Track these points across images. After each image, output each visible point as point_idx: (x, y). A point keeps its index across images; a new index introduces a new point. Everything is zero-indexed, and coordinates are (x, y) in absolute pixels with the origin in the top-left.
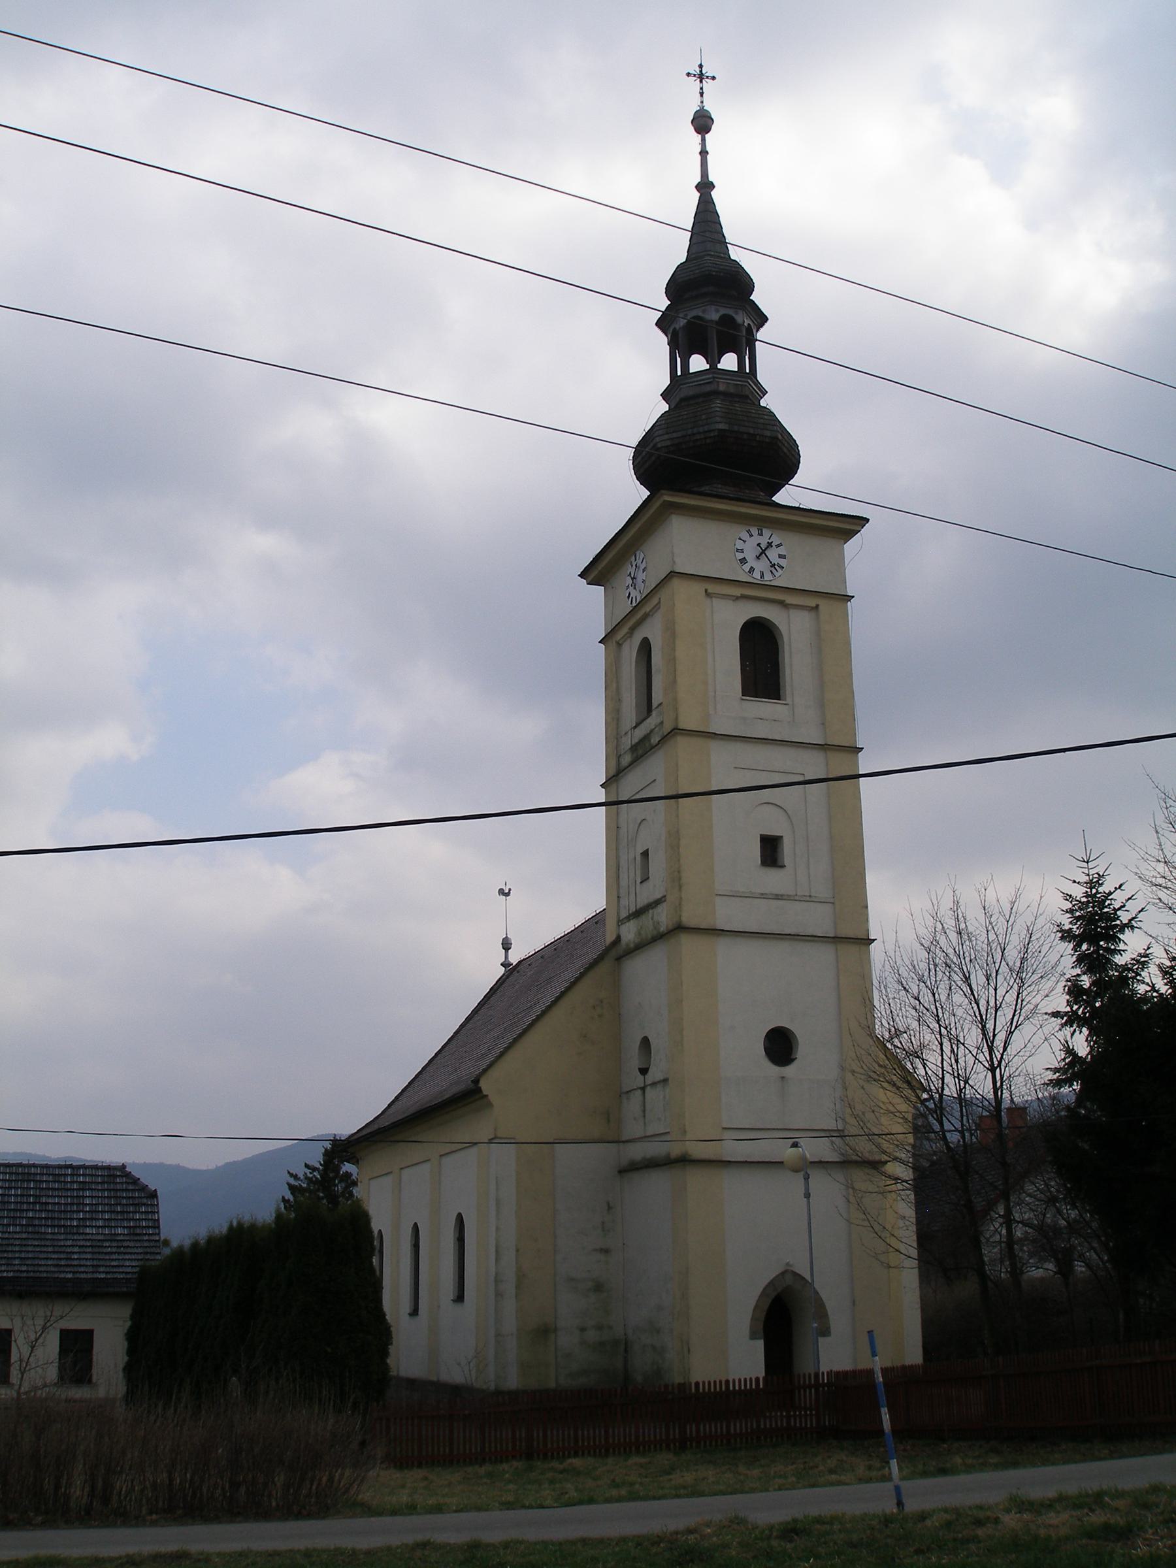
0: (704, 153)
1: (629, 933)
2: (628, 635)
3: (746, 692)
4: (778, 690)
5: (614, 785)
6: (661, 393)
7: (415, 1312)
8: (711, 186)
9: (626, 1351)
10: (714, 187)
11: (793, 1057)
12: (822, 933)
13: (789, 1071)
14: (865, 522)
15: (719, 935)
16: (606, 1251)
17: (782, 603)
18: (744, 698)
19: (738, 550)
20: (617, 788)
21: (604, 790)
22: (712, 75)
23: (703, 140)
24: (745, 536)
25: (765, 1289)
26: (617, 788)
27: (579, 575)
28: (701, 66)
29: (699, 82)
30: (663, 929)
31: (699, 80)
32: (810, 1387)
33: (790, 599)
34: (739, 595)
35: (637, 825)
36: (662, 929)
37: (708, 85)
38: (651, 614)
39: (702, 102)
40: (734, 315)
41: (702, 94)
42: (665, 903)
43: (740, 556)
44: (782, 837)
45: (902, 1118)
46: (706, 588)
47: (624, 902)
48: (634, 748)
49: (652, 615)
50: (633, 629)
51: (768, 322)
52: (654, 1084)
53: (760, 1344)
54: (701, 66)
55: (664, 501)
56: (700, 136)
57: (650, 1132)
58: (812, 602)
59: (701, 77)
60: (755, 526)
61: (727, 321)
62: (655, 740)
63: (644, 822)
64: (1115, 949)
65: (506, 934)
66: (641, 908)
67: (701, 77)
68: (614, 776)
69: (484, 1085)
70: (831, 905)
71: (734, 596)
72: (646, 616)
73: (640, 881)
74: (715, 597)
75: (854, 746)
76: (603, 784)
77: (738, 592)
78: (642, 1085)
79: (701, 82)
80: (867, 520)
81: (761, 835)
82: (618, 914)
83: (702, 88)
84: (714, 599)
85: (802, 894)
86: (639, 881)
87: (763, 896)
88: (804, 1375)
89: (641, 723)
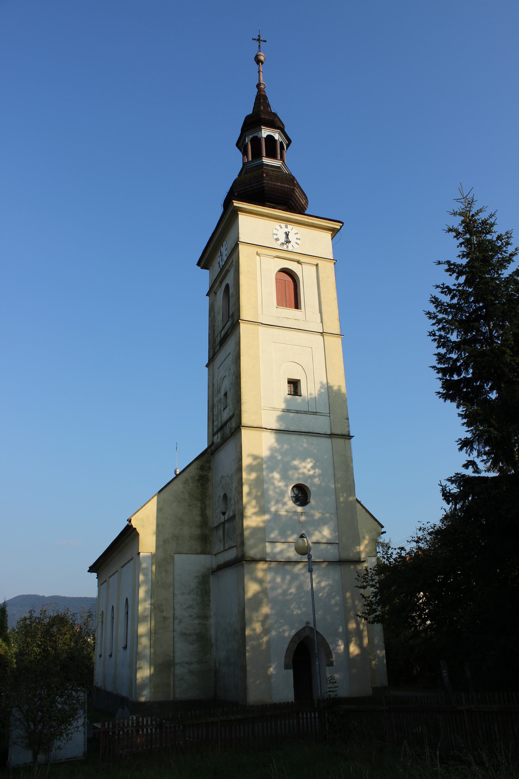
2: (219, 286)
4: (298, 307)
7: (125, 648)
11: (308, 501)
12: (324, 432)
18: (277, 307)
24: (278, 227)
28: (259, 36)
40: (273, 135)
43: (275, 237)
44: (300, 380)
45: (214, 352)
49: (230, 270)
50: (221, 282)
53: (291, 672)
54: (259, 36)
58: (315, 261)
63: (226, 377)
64: (367, 606)
69: (134, 524)
70: (329, 417)
73: (223, 409)
79: (259, 43)
83: (259, 46)
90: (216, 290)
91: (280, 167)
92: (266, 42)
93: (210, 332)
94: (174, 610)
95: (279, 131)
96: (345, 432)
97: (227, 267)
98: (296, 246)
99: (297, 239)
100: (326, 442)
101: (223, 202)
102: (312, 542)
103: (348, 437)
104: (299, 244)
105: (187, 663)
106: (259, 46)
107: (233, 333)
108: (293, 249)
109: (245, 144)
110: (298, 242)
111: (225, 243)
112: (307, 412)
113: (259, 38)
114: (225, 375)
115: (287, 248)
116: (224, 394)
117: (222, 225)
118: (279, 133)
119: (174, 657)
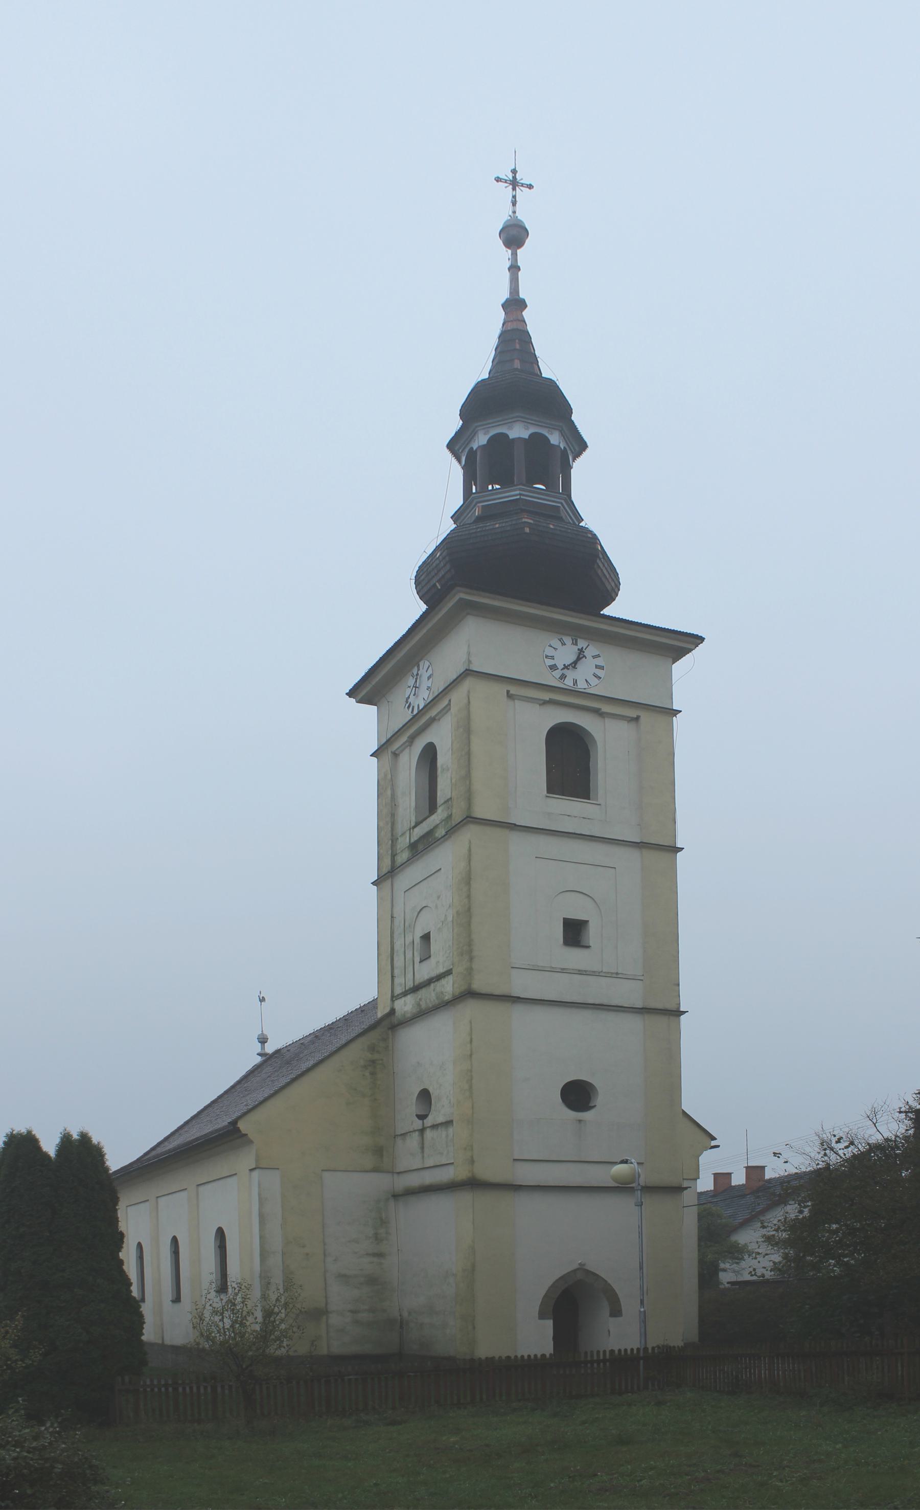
0: (514, 269)
1: (405, 1006)
3: (550, 790)
4: (589, 793)
5: (388, 882)
6: (451, 515)
7: (177, 1299)
8: (522, 305)
9: (401, 1327)
10: (526, 306)
11: (591, 1104)
13: (586, 1115)
14: (700, 641)
15: (514, 1002)
16: (380, 1255)
17: (597, 712)
18: (548, 795)
19: (547, 657)
20: (392, 885)
21: (376, 887)
22: (528, 183)
23: (514, 255)
25: (557, 1281)
26: (392, 885)
27: (347, 694)
28: (514, 172)
29: (511, 190)
30: (447, 997)
31: (511, 187)
32: (598, 1362)
33: (606, 708)
34: (548, 699)
35: (416, 914)
36: (446, 998)
37: (521, 193)
38: (437, 718)
39: (514, 212)
40: (547, 435)
41: (514, 203)
42: (451, 975)
43: (549, 662)
44: (588, 921)
46: (509, 689)
47: (399, 980)
48: (413, 846)
49: (439, 720)
50: (412, 739)
51: (588, 451)
52: (434, 1127)
53: (549, 1323)
54: (514, 172)
55: (461, 599)
56: (510, 251)
57: (430, 1162)
58: (632, 713)
59: (515, 183)
60: (569, 635)
61: (538, 441)
62: (440, 832)
65: (261, 1005)
66: (420, 984)
67: (515, 183)
68: (389, 872)
71: (542, 700)
72: (433, 720)
74: (519, 700)
75: (674, 846)
76: (374, 882)
77: (546, 696)
78: (420, 1127)
79: (514, 189)
80: (701, 639)
81: (564, 918)
82: (392, 991)
83: (514, 197)
84: (516, 701)
85: (606, 971)
86: (417, 959)
87: (563, 971)
88: (592, 1352)
89: (421, 822)
90: (398, 748)
91: (558, 507)
92: (532, 190)
93: (381, 824)
94: (325, 1244)
95: (561, 424)
96: (671, 1006)
97: (433, 713)
98: (593, 681)
99: (597, 667)
100: (634, 1023)
101: (415, 574)
102: (638, 1162)
103: (678, 1013)
104: (600, 678)
105: (351, 1311)
106: (514, 197)
107: (450, 837)
108: (587, 687)
109: (472, 448)
110: (600, 673)
111: (428, 663)
112: (599, 972)
113: (514, 178)
114: (424, 905)
115: (574, 685)
116: (421, 935)
117: (424, 631)
118: (561, 431)
119: (327, 1304)
